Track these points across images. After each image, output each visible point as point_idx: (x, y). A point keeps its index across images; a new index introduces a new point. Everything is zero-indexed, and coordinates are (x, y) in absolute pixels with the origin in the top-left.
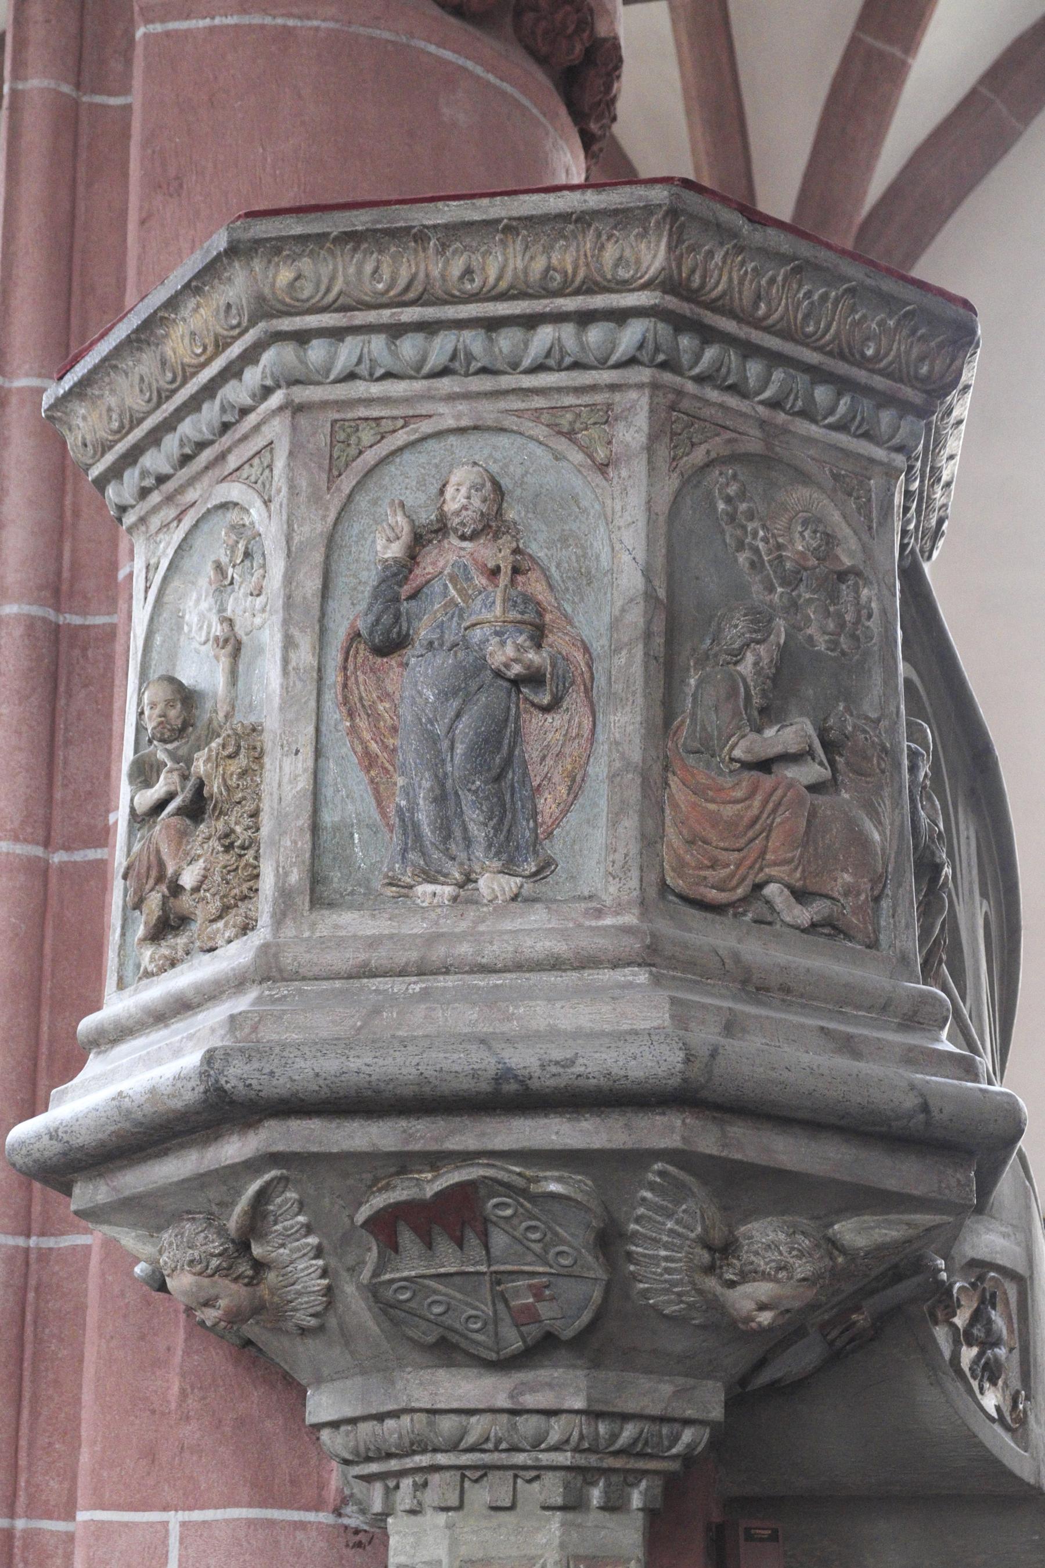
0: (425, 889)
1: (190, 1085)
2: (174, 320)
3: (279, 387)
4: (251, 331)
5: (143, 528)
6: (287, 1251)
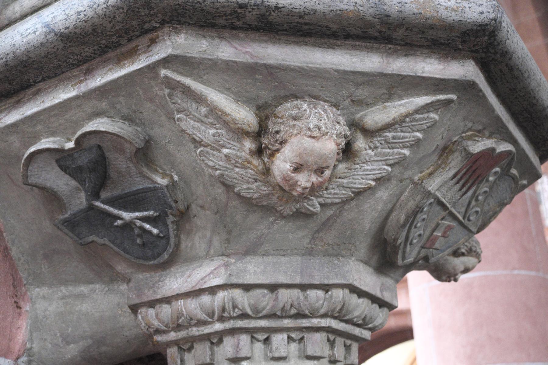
6: (373, 153)
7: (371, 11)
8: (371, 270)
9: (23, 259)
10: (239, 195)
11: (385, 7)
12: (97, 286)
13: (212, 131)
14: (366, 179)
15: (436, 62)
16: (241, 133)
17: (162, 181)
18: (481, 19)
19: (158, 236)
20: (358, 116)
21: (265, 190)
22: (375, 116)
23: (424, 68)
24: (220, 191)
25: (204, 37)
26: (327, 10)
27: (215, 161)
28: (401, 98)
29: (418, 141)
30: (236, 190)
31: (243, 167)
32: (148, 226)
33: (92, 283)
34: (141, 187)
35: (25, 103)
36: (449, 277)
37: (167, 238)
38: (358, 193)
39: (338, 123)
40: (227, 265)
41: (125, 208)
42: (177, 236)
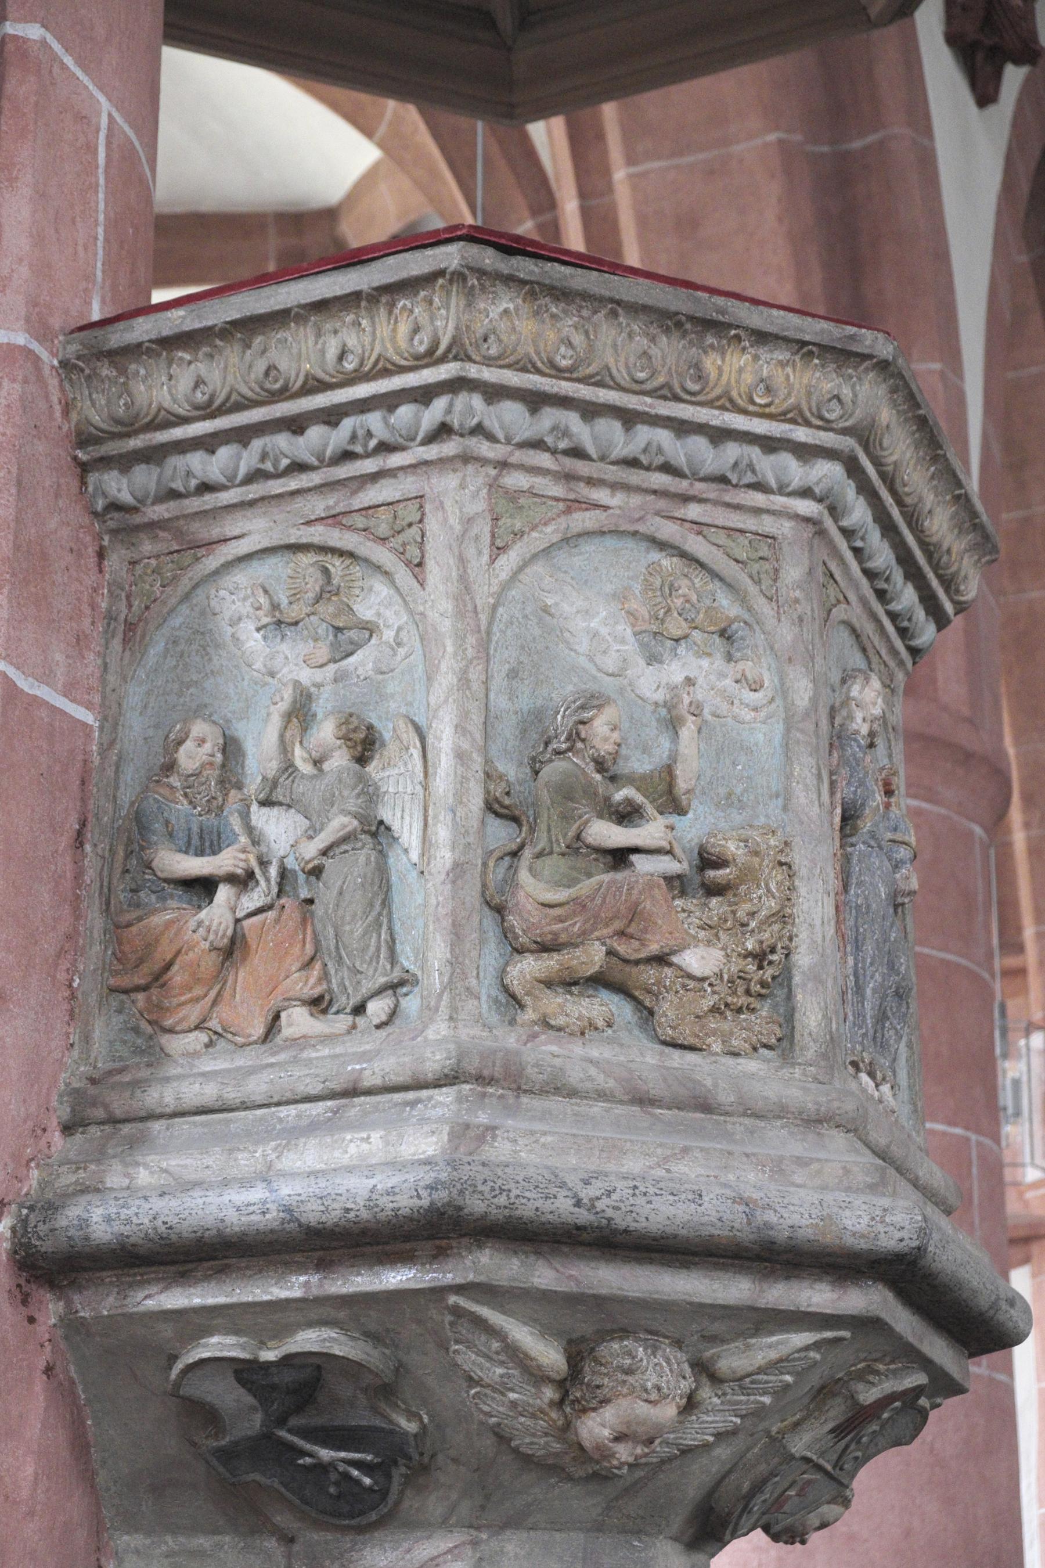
0: (864, 1077)
1: (898, 1235)
2: (744, 349)
3: (820, 500)
4: (831, 434)
5: (494, 472)
7: (751, 1237)
8: (679, 1547)
9: (113, 1489)
10: (516, 1451)
11: (771, 1233)
12: (227, 1539)
13: (500, 1371)
14: (703, 1434)
15: (829, 1288)
16: (536, 1376)
17: (411, 1427)
18: (901, 1247)
19: (370, 1489)
20: (708, 1354)
21: (557, 1447)
22: (733, 1360)
23: (810, 1298)
24: (489, 1442)
25: (516, 1253)
26: (692, 1234)
27: (495, 1408)
28: (772, 1333)
29: (787, 1386)
30: (513, 1444)
31: (533, 1416)
32: (355, 1473)
33: (220, 1533)
34: (364, 1423)
35: (198, 1281)
36: (793, 1537)
37: (384, 1494)
38: (686, 1451)
39: (684, 1378)
40: (475, 1543)
41: (325, 1444)
42: (402, 1493)
